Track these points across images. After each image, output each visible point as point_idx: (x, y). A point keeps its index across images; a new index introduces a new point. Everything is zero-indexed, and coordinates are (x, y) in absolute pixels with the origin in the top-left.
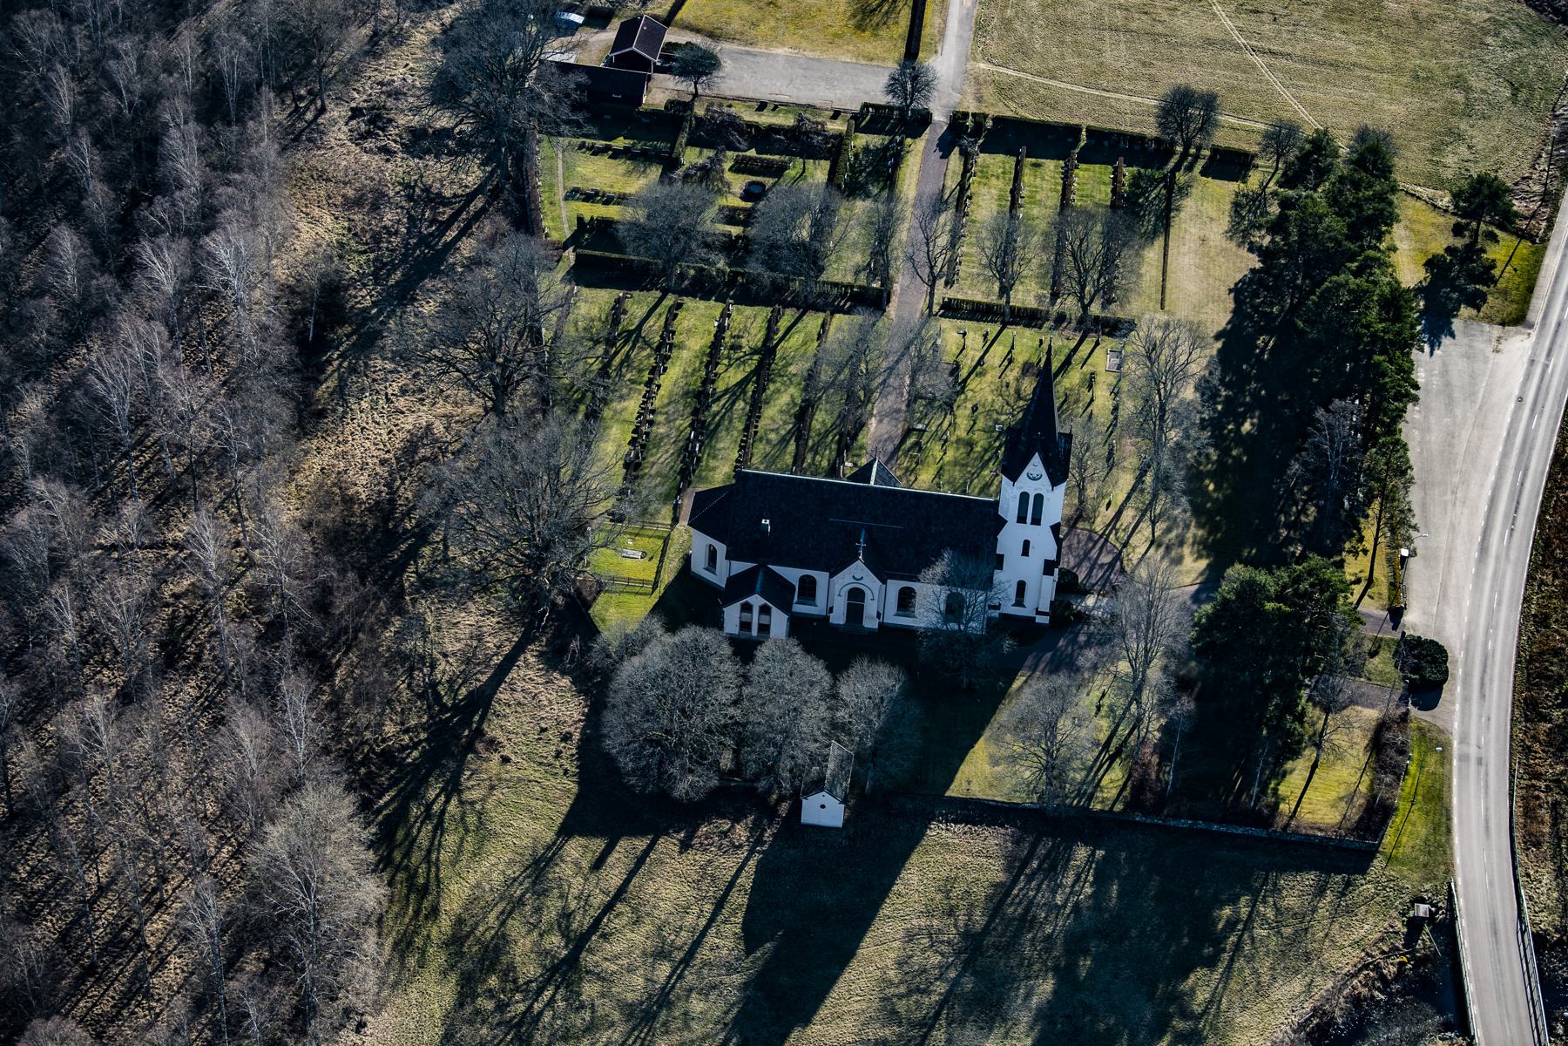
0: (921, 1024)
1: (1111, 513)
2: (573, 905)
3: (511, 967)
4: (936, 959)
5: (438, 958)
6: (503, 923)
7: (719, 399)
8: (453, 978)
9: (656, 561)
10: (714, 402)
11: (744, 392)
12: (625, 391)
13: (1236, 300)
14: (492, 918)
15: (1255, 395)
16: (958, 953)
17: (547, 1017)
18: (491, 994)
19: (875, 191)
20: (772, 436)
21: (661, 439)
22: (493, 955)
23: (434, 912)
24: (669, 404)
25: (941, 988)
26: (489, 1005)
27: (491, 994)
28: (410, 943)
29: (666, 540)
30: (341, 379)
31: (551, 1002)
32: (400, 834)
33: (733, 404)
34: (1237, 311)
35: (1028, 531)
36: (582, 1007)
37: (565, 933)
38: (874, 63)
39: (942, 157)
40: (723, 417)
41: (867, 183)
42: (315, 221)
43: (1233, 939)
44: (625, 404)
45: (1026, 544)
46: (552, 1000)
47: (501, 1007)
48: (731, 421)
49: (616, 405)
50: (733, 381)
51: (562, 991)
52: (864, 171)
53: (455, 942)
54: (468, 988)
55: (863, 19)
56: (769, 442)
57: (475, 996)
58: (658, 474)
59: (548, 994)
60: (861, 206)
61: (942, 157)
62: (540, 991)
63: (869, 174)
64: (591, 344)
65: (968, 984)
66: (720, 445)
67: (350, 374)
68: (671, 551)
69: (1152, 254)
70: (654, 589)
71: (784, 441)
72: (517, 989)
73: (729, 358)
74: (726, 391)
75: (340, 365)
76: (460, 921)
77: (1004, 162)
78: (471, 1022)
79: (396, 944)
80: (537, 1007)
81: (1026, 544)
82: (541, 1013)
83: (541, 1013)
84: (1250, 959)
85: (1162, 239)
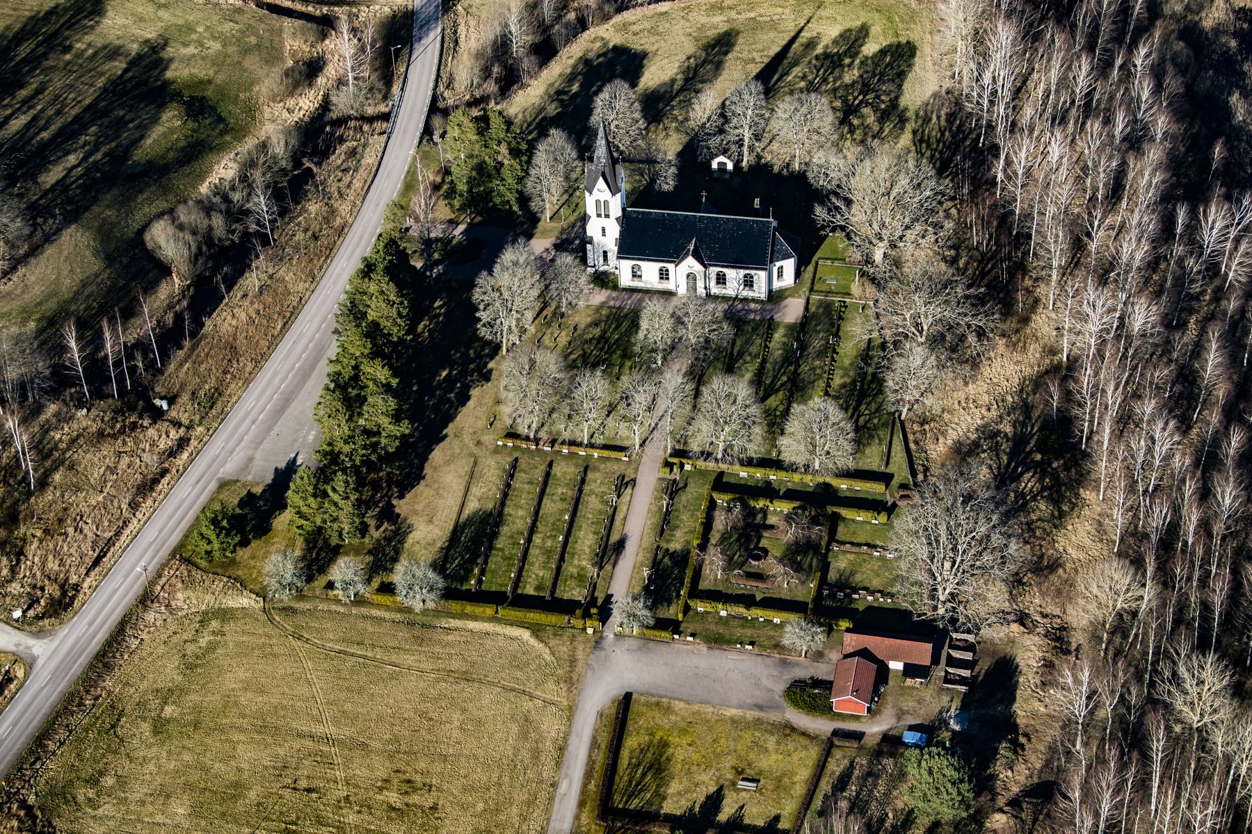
0: (685, 90)
1: (545, 313)
2: (849, 136)
3: (875, 112)
4: (675, 112)
5: (910, 114)
6: (881, 128)
7: (782, 385)
8: (901, 107)
9: (818, 276)
10: (786, 382)
11: (766, 390)
12: (843, 391)
13: (422, 468)
14: (887, 130)
15: (432, 396)
16: (665, 114)
17: (856, 94)
18: (883, 102)
19: (666, 560)
20: (748, 359)
21: (817, 356)
22: (883, 117)
23: (914, 132)
24: (814, 381)
25: (674, 103)
26: (883, 98)
27: (883, 102)
28: (924, 120)
29: (811, 290)
30: (1030, 418)
31: (855, 98)
32: (938, 164)
33: (773, 381)
34: (424, 459)
35: (603, 222)
36: (840, 97)
37: (851, 125)
38: (654, 700)
39: (612, 595)
40: (779, 371)
41: (672, 567)
42: (1080, 548)
43: (531, 128)
44: (842, 381)
45: (603, 229)
46: (855, 100)
47: (878, 97)
48: (774, 369)
49: (847, 380)
50: (773, 398)
51: (850, 103)
52: (673, 580)
53: (903, 120)
54: (894, 104)
55: (661, 755)
56: (750, 354)
57: (890, 100)
58: (818, 332)
59: (856, 102)
60: (676, 546)
61: (612, 595)
62: (861, 102)
63: (669, 576)
64: (869, 425)
65: (661, 105)
66: (780, 352)
67: (1024, 421)
68: (808, 284)
69: (472, 506)
70: (817, 263)
71: (741, 355)
72: (871, 104)
73: (776, 416)
74: (777, 391)
75: (1032, 429)
76: (902, 129)
77: (564, 591)
78: (890, 91)
79: (930, 119)
80: (861, 97)
81: (603, 229)
82: (859, 94)
83: (859, 94)
84: (525, 121)
85: (461, 520)
